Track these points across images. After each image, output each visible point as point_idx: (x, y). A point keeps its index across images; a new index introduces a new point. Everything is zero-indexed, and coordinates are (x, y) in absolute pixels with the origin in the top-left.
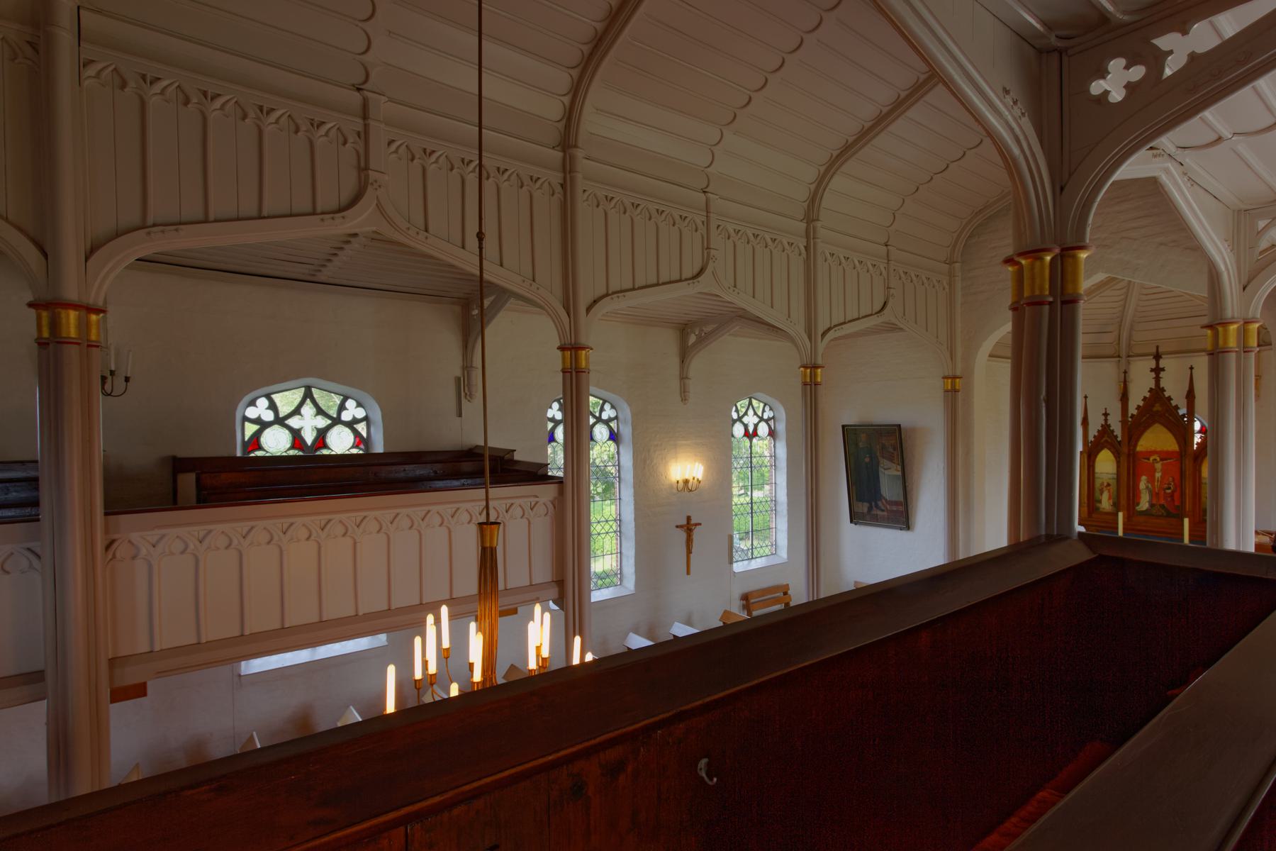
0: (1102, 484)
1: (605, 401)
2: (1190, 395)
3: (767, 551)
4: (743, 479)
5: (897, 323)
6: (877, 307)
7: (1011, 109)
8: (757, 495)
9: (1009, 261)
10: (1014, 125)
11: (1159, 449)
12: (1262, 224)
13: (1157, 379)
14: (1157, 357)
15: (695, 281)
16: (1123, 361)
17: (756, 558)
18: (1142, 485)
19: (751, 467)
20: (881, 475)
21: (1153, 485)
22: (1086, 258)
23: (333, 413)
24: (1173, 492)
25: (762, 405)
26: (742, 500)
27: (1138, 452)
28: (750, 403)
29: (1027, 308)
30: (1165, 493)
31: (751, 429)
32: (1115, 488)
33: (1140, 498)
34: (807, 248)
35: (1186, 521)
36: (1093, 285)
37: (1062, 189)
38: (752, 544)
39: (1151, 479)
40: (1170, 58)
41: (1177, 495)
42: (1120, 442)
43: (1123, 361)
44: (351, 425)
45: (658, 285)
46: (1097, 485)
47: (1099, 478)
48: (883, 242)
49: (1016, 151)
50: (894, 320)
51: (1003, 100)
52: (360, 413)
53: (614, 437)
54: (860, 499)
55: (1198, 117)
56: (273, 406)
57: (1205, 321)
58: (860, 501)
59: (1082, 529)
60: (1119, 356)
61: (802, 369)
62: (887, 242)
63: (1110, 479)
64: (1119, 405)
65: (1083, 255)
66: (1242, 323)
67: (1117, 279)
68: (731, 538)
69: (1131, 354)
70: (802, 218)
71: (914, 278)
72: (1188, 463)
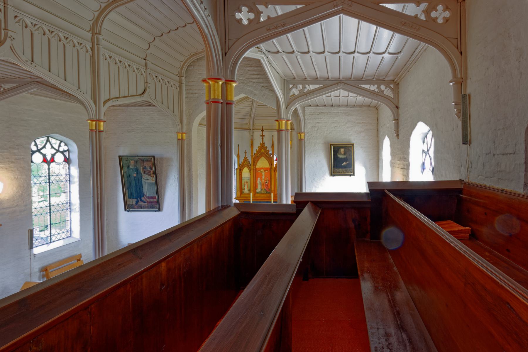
0: (245, 182)
1: (61, 142)
2: (273, 146)
3: (63, 236)
4: (43, 191)
5: (152, 102)
6: (140, 91)
7: (204, 11)
8: (54, 200)
9: (204, 81)
10: (205, 19)
11: (263, 167)
12: (291, 86)
13: (263, 139)
14: (262, 131)
15: (142, 96)
16: (251, 131)
17: (54, 241)
18: (258, 182)
19: (49, 182)
20: (143, 182)
21: (262, 181)
22: (236, 86)
23: (57, 149)
24: (268, 183)
25: (58, 142)
26: (41, 204)
27: (257, 168)
28: (48, 140)
29: (212, 104)
30: (266, 184)
31: (49, 158)
32: (249, 183)
33: (258, 186)
34: (92, 49)
35: (272, 194)
36: (240, 98)
37: (226, 54)
38: (51, 233)
39: (261, 179)
40: (262, 14)
41: (269, 185)
42: (250, 164)
43: (251, 131)
44: (62, 152)
45: (128, 96)
46: (243, 183)
47: (244, 179)
48: (143, 58)
49: (207, 31)
50: (150, 100)
51: (200, 5)
52: (66, 148)
53: (67, 160)
54: (131, 197)
55: (271, 41)
56: (36, 145)
57: (276, 119)
58: (131, 198)
59: (237, 202)
60: (250, 129)
61: (89, 121)
62: (146, 58)
63: (247, 180)
64: (250, 149)
65: (234, 85)
66: (286, 120)
67: (249, 97)
68: (31, 232)
69: (254, 129)
70: (89, 30)
71: (161, 80)
72: (272, 172)
